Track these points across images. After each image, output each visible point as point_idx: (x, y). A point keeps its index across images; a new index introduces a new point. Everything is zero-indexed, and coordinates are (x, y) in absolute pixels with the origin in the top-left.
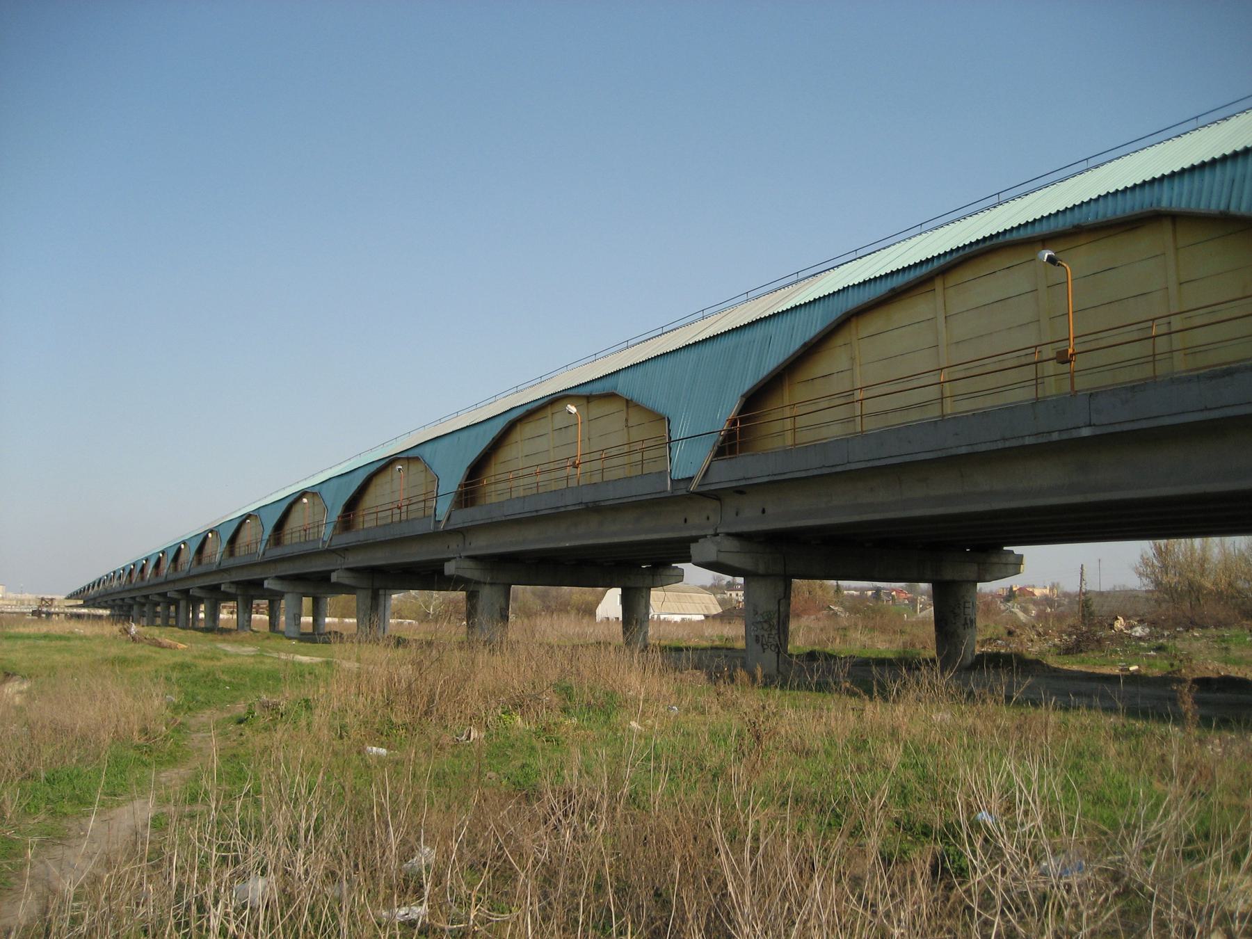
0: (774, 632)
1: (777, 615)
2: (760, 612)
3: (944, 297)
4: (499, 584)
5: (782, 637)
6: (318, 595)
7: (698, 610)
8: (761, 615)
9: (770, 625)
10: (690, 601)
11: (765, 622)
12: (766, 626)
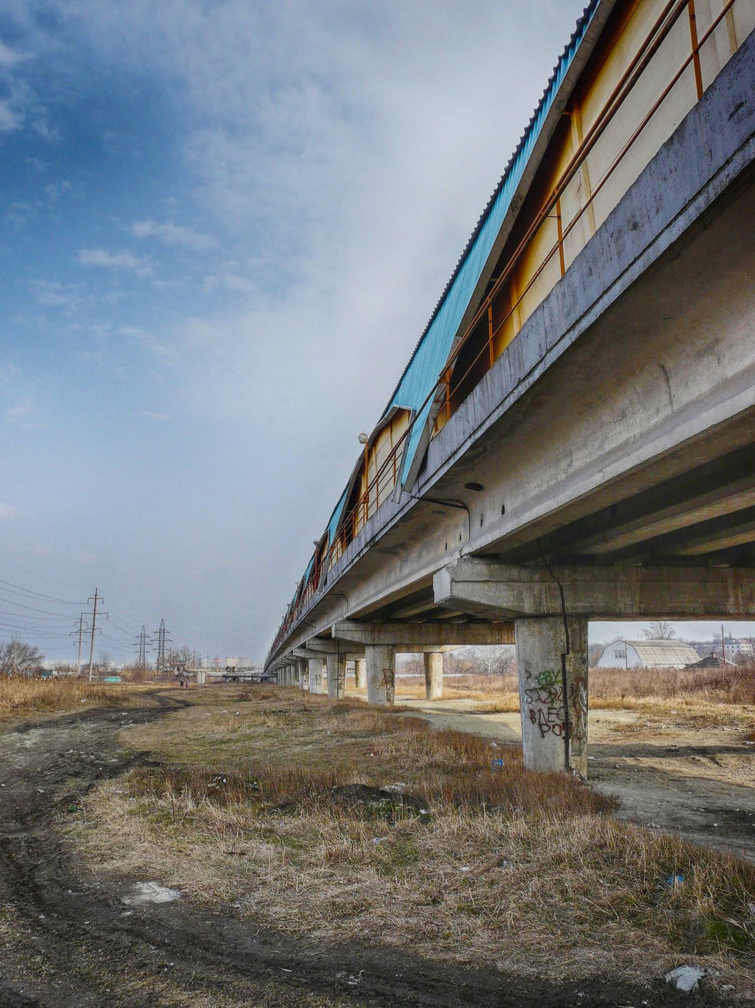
0: (558, 704)
1: (560, 678)
2: (535, 673)
3: (519, 313)
4: (383, 645)
5: (572, 711)
6: (358, 660)
7: (681, 661)
8: (536, 678)
9: (550, 693)
10: (673, 653)
11: (543, 688)
12: (544, 695)
